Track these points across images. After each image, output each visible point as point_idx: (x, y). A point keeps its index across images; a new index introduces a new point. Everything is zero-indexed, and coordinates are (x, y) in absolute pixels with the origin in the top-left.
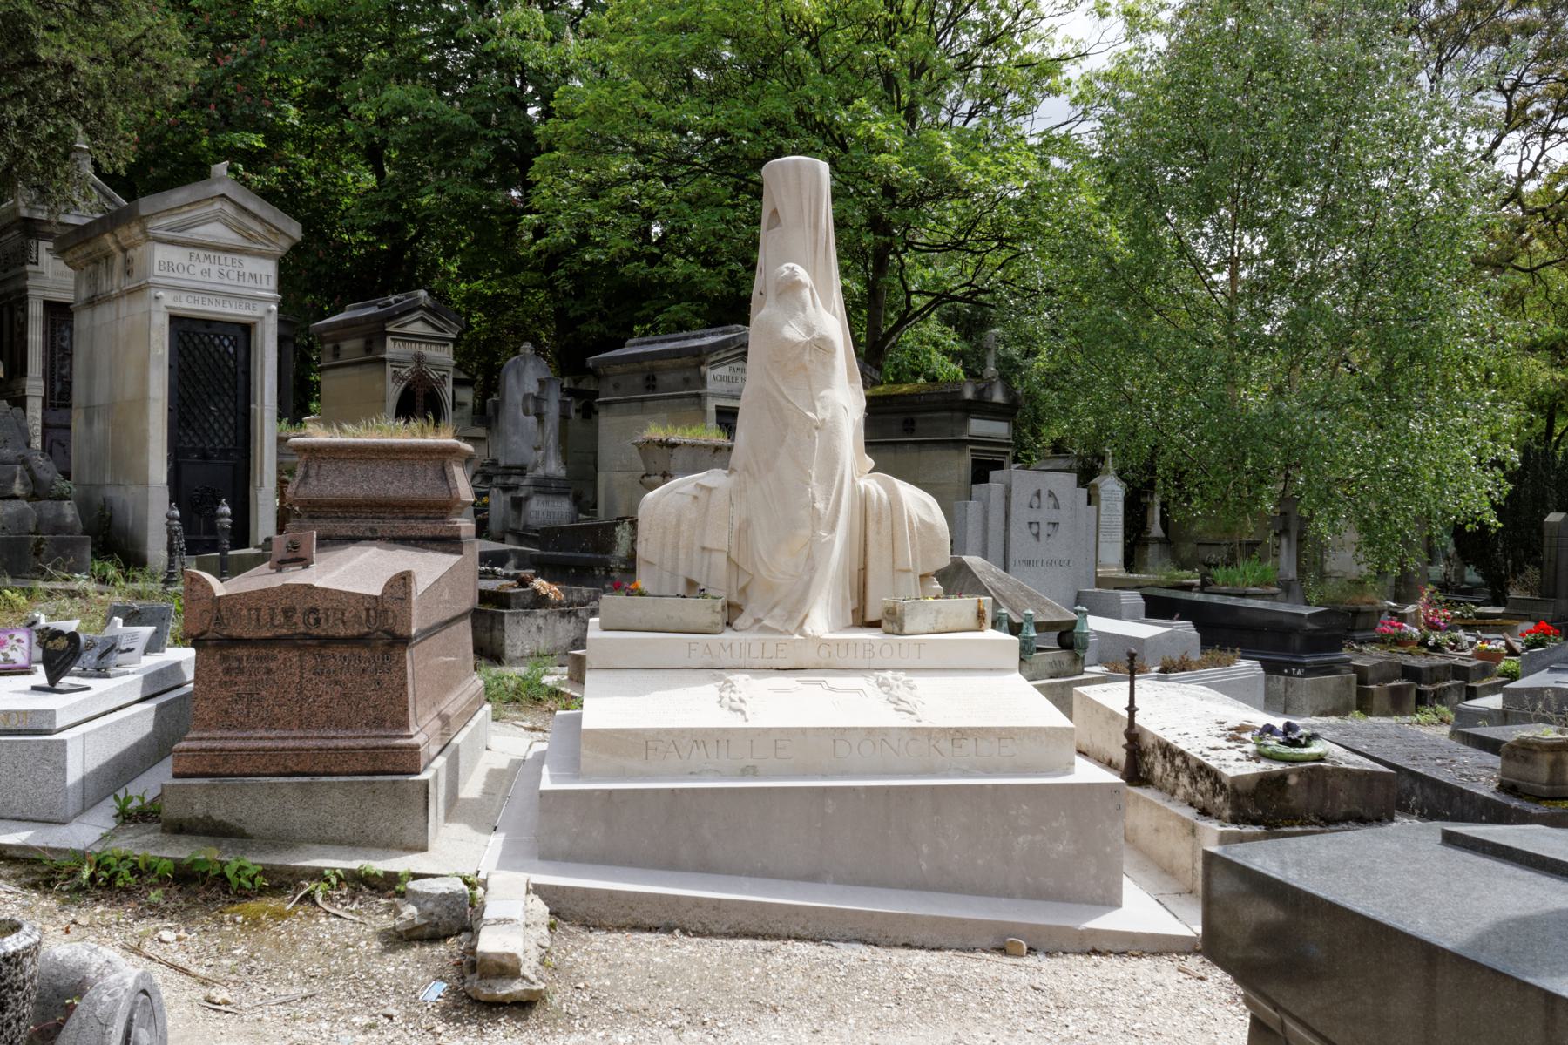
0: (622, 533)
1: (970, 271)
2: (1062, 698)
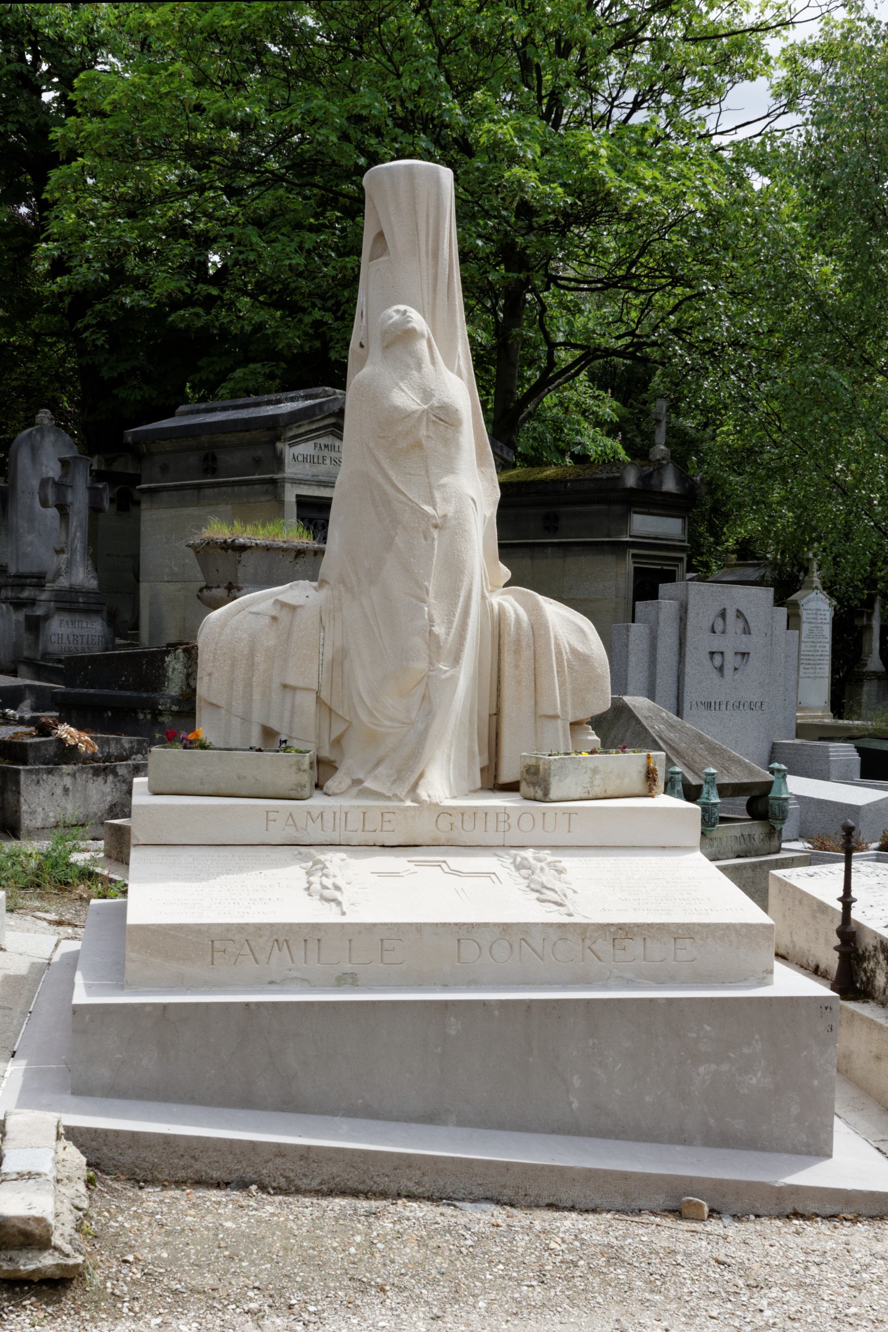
0: (175, 665)
1: (634, 314)
2: (754, 885)
